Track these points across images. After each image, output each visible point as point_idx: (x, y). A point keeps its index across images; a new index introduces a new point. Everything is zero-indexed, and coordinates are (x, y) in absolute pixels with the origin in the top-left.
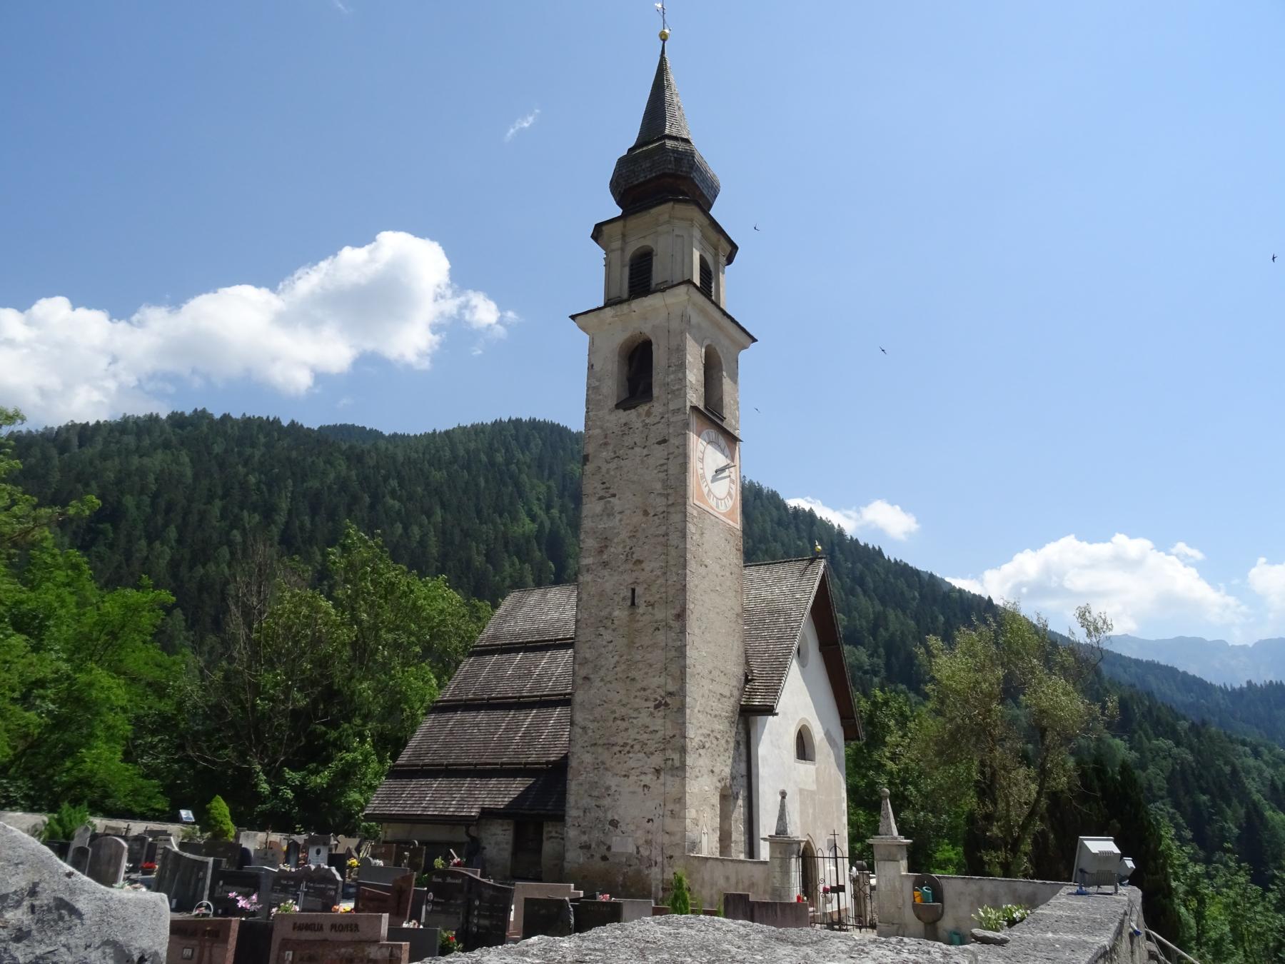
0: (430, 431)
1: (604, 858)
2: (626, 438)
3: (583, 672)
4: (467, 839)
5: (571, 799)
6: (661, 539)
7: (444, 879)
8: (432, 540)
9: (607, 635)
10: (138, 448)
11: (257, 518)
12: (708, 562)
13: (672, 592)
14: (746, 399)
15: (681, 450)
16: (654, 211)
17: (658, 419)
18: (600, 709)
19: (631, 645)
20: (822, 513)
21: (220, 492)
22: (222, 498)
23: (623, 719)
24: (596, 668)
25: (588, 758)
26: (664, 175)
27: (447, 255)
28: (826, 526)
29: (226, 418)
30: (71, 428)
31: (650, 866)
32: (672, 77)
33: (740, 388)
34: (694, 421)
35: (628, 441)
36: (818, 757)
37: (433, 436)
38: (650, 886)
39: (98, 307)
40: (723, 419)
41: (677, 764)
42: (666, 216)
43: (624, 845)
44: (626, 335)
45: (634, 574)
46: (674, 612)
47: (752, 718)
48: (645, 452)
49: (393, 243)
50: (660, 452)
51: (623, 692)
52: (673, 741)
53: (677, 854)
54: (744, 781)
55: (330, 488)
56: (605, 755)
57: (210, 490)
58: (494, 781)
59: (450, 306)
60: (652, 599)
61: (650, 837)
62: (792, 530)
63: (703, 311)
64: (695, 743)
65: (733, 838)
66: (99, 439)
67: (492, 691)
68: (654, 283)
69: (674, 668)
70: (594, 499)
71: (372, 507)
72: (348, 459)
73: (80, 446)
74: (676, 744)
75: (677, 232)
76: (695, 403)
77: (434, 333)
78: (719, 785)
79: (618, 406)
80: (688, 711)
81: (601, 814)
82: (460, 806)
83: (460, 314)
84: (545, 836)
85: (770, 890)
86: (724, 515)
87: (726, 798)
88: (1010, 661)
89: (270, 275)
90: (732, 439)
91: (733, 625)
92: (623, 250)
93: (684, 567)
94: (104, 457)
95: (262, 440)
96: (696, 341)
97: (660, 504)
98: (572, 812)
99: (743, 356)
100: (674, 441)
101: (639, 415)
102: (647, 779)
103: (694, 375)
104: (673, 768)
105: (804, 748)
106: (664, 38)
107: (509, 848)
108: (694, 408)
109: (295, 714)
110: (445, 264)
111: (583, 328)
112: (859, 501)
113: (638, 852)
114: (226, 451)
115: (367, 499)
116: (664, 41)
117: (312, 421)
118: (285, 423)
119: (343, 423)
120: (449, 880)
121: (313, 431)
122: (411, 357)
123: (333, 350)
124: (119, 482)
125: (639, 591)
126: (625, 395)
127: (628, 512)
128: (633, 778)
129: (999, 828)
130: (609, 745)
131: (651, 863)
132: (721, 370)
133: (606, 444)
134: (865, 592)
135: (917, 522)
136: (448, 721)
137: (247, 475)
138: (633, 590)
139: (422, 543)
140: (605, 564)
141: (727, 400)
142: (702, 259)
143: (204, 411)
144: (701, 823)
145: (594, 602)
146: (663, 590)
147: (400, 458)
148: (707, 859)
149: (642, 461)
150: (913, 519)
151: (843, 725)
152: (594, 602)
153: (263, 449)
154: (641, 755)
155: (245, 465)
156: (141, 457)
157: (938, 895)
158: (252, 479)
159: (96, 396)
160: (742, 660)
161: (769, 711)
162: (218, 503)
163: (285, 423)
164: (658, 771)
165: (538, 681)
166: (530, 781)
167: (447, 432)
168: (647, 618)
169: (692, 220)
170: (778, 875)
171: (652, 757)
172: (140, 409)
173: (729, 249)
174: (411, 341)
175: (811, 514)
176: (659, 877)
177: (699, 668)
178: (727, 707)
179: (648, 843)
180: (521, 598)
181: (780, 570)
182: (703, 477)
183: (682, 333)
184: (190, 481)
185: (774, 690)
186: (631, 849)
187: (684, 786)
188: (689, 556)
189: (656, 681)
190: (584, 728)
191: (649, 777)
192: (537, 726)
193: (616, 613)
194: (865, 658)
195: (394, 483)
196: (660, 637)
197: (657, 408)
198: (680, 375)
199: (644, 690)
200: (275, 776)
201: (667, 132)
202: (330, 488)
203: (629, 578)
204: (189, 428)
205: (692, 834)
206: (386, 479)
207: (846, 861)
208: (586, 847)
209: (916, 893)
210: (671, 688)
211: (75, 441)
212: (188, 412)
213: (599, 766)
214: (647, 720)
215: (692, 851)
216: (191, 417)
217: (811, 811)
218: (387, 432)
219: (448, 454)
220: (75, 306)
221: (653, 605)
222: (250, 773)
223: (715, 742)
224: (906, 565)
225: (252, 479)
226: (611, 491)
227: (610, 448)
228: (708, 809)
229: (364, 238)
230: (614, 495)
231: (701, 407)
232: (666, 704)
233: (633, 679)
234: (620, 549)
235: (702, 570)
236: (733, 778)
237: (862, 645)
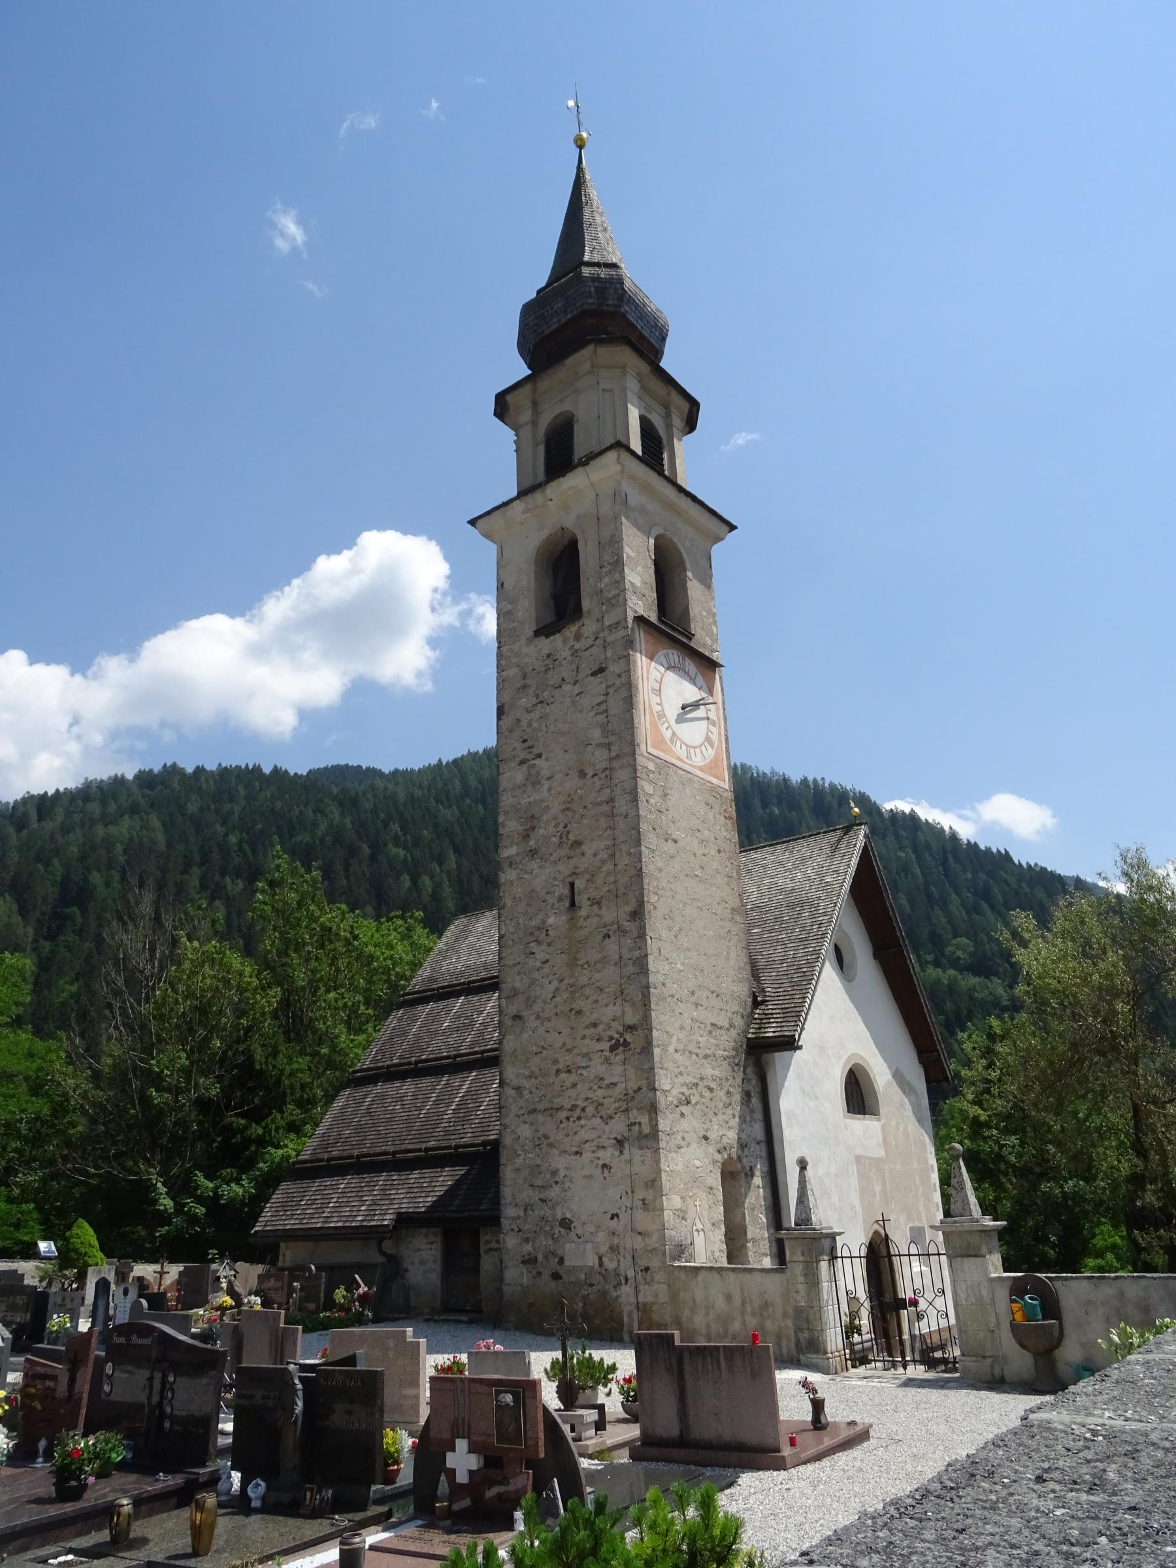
0: (434, 762)
1: (556, 1276)
2: (550, 673)
3: (512, 1010)
4: (381, 1259)
5: (507, 1192)
6: (606, 808)
7: (129, 1339)
8: (447, 891)
9: (541, 953)
10: (103, 815)
11: (241, 884)
12: (676, 834)
13: (623, 880)
14: (722, 607)
15: (623, 679)
16: (570, 361)
17: (590, 642)
18: (537, 1059)
19: (573, 963)
20: (927, 814)
21: (197, 858)
22: (200, 865)
23: (569, 1071)
24: (530, 1002)
25: (525, 1131)
26: (584, 314)
27: (447, 558)
28: (935, 831)
29: (199, 770)
30: (28, 800)
31: (620, 1284)
32: (593, 191)
33: (716, 594)
34: (641, 637)
35: (553, 678)
36: (883, 1110)
37: (438, 769)
38: (621, 1314)
39: (59, 662)
40: (690, 636)
41: (646, 1130)
42: (587, 366)
43: (581, 1255)
44: (545, 534)
45: (572, 862)
46: (629, 909)
47: (766, 1056)
48: (577, 689)
49: (379, 546)
50: (596, 686)
51: (566, 1032)
52: (639, 1096)
53: (655, 1263)
54: (762, 1150)
55: (322, 840)
56: (548, 1125)
57: (185, 857)
58: (415, 1174)
59: (449, 616)
60: (597, 895)
61: (616, 1241)
62: (891, 838)
63: (645, 488)
64: (672, 1098)
65: (749, 1236)
66: (60, 811)
67: (423, 1050)
68: (576, 459)
69: (633, 991)
70: (513, 765)
71: (373, 858)
72: (341, 804)
73: (40, 819)
74: (643, 1101)
75: (603, 385)
76: (641, 612)
77: (433, 648)
78: (718, 1157)
79: (538, 633)
80: (657, 1051)
81: (548, 1212)
82: (370, 1214)
83: (464, 625)
84: (483, 1247)
85: (790, 1309)
86: (701, 769)
87: (733, 1177)
88: (1144, 938)
89: (240, 602)
90: (708, 665)
91: (728, 925)
92: (534, 423)
93: (638, 843)
94: (66, 829)
95: (242, 791)
96: (639, 528)
97: (599, 757)
98: (509, 1212)
99: (717, 550)
100: (614, 668)
101: (565, 641)
102: (607, 1156)
103: (638, 576)
104: (642, 1137)
105: (858, 1095)
106: (580, 144)
107: (438, 1267)
108: (640, 620)
109: (203, 1105)
110: (444, 568)
111: (488, 536)
112: (968, 798)
113: (601, 1265)
114: (201, 810)
115: (366, 850)
116: (581, 147)
117: (298, 766)
118: (267, 770)
119: (335, 763)
120: (135, 1340)
121: (300, 777)
122: (409, 678)
123: (323, 683)
124: (82, 858)
125: (579, 884)
126: (549, 618)
127: (558, 777)
128: (587, 1156)
129: (1155, 1192)
130: (552, 1111)
131: (620, 1280)
132: (685, 571)
133: (525, 687)
134: (993, 908)
135: (1054, 816)
136: (365, 1097)
137: (226, 835)
138: (572, 885)
139: (436, 896)
140: (533, 853)
141: (695, 610)
142: (644, 421)
143: (174, 765)
144: (691, 1214)
145: (521, 908)
146: (611, 879)
147: (402, 797)
148: (697, 1269)
149: (574, 703)
150: (1049, 812)
151: (921, 1061)
152: (521, 908)
153: (243, 802)
154: (597, 1121)
155: (224, 823)
156: (106, 825)
157: (1051, 1307)
158: (233, 839)
159: (57, 762)
160: (746, 974)
161: (789, 1044)
162: (196, 871)
163: (267, 770)
164: (620, 1143)
165: (481, 1033)
166: (461, 1171)
167: (455, 761)
168: (594, 921)
169: (623, 368)
170: (802, 1288)
171: (612, 1123)
172: (103, 772)
173: (686, 406)
174: (406, 660)
175: (913, 817)
176: (632, 1300)
177: (672, 988)
178: (726, 1042)
179: (614, 1249)
180: (468, 925)
181: (803, 848)
182: (662, 715)
183: (616, 518)
184: (164, 848)
185: (796, 1014)
186: (591, 1261)
187: (657, 1162)
188: (644, 827)
189: (611, 1011)
190: (518, 1089)
191: (610, 1151)
192: (474, 1095)
193: (551, 920)
194: (1000, 991)
195: (395, 827)
196: (612, 947)
197: (589, 626)
198: (617, 576)
199: (595, 1025)
200: (181, 1187)
201: (586, 258)
202: (322, 840)
203: (564, 869)
204: (159, 788)
205: (675, 1231)
206: (386, 824)
207: (944, 1258)
208: (530, 1261)
209: (1015, 1306)
210: (630, 1019)
211: (34, 816)
212: (157, 768)
213: (542, 1142)
214: (602, 1070)
215: (678, 1257)
216: (161, 774)
217: (878, 1188)
218: (386, 770)
219: (457, 784)
220: (32, 661)
221: (599, 903)
222: (149, 1187)
223: (707, 1094)
224: (1044, 870)
225: (233, 839)
226: (536, 751)
227: (531, 691)
228: (702, 1194)
229: (342, 541)
230: (539, 756)
231: (653, 617)
232: (626, 1044)
233: (579, 1012)
234: (551, 829)
235: (669, 847)
236: (742, 1146)
237: (995, 974)
